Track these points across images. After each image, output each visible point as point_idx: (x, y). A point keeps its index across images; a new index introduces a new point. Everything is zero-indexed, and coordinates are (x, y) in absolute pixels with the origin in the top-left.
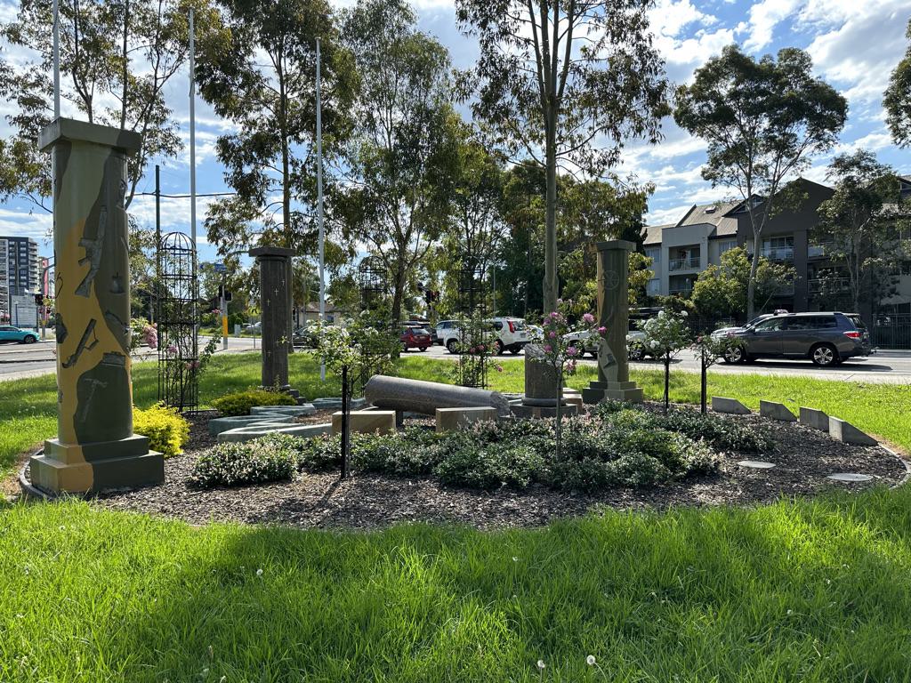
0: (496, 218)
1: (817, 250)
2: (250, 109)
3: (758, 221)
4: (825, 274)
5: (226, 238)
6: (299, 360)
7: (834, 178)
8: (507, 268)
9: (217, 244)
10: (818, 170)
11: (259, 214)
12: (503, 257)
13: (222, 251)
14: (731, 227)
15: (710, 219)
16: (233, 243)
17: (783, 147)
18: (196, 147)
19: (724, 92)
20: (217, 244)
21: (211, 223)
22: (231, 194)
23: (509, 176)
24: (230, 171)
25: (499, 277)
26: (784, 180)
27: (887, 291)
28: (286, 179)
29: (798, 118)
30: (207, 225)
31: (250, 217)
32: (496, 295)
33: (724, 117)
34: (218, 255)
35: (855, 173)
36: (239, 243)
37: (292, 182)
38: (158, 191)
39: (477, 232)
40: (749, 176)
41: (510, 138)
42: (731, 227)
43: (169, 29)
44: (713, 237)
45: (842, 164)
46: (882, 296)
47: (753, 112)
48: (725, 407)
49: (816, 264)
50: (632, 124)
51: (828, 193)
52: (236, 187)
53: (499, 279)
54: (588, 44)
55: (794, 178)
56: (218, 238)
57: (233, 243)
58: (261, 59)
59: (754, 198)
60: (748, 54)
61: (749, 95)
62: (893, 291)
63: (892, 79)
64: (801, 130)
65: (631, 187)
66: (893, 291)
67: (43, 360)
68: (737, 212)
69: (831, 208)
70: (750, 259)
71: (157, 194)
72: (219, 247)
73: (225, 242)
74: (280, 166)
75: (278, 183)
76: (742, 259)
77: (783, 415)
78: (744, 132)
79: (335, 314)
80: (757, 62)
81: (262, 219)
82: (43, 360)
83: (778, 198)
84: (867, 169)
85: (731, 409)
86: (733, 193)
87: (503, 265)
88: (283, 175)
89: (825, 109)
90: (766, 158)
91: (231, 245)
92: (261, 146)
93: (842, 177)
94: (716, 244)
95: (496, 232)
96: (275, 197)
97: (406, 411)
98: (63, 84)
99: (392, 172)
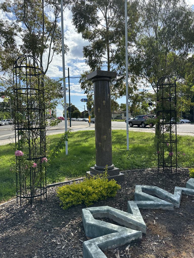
5: (87, 87)
6: (115, 134)
9: (84, 89)
13: (86, 92)
16: (90, 89)
20: (84, 89)
24: (87, 59)
28: (108, 59)
30: (80, 82)
34: (84, 93)
36: (92, 89)
37: (111, 61)
43: (167, 25)
52: (90, 64)
56: (84, 87)
57: (90, 89)
67: (58, 129)
72: (85, 91)
73: (87, 89)
75: (105, 63)
79: (122, 114)
82: (58, 129)
88: (107, 60)
91: (89, 90)
98: (60, 61)
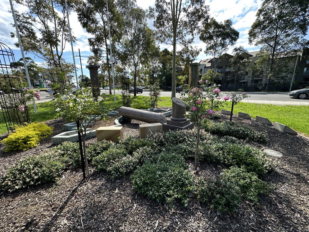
0: (159, 63)
1: (228, 70)
2: (97, 31)
3: (216, 63)
4: (230, 75)
7: (234, 53)
8: (161, 74)
10: (230, 51)
11: (101, 60)
12: (160, 72)
14: (209, 65)
15: (205, 63)
17: (223, 45)
18: (231, 111)
19: (211, 32)
21: (89, 62)
22: (93, 54)
23: (161, 53)
25: (160, 76)
26: (222, 54)
27: (242, 79)
29: (228, 37)
31: (98, 60)
32: (159, 80)
33: (211, 38)
35: (238, 52)
38: (80, 55)
39: (155, 66)
40: (215, 52)
41: (164, 36)
42: (209, 65)
44: (205, 67)
45: (236, 50)
46: (241, 80)
47: (218, 36)
48: (226, 113)
49: (227, 73)
50: (197, 31)
51: (232, 57)
52: (93, 52)
53: (159, 76)
54: (185, 6)
55: (225, 53)
58: (98, 16)
59: (215, 58)
60: (217, 21)
61: (217, 32)
62: (244, 79)
63: (251, 27)
64: (227, 41)
65: (195, 50)
66: (244, 79)
68: (211, 61)
69: (232, 60)
70: (213, 72)
71: (80, 56)
74: (105, 46)
76: (212, 72)
77: (247, 117)
78: (214, 42)
80: (219, 24)
81: (101, 61)
83: (221, 57)
84: (241, 50)
85: (228, 113)
86: (211, 57)
87: (160, 73)
89: (234, 35)
90: (219, 48)
92: (99, 40)
93: (236, 53)
94: (206, 69)
95: (159, 66)
96: (104, 55)
97: (135, 119)
99: (132, 46)
